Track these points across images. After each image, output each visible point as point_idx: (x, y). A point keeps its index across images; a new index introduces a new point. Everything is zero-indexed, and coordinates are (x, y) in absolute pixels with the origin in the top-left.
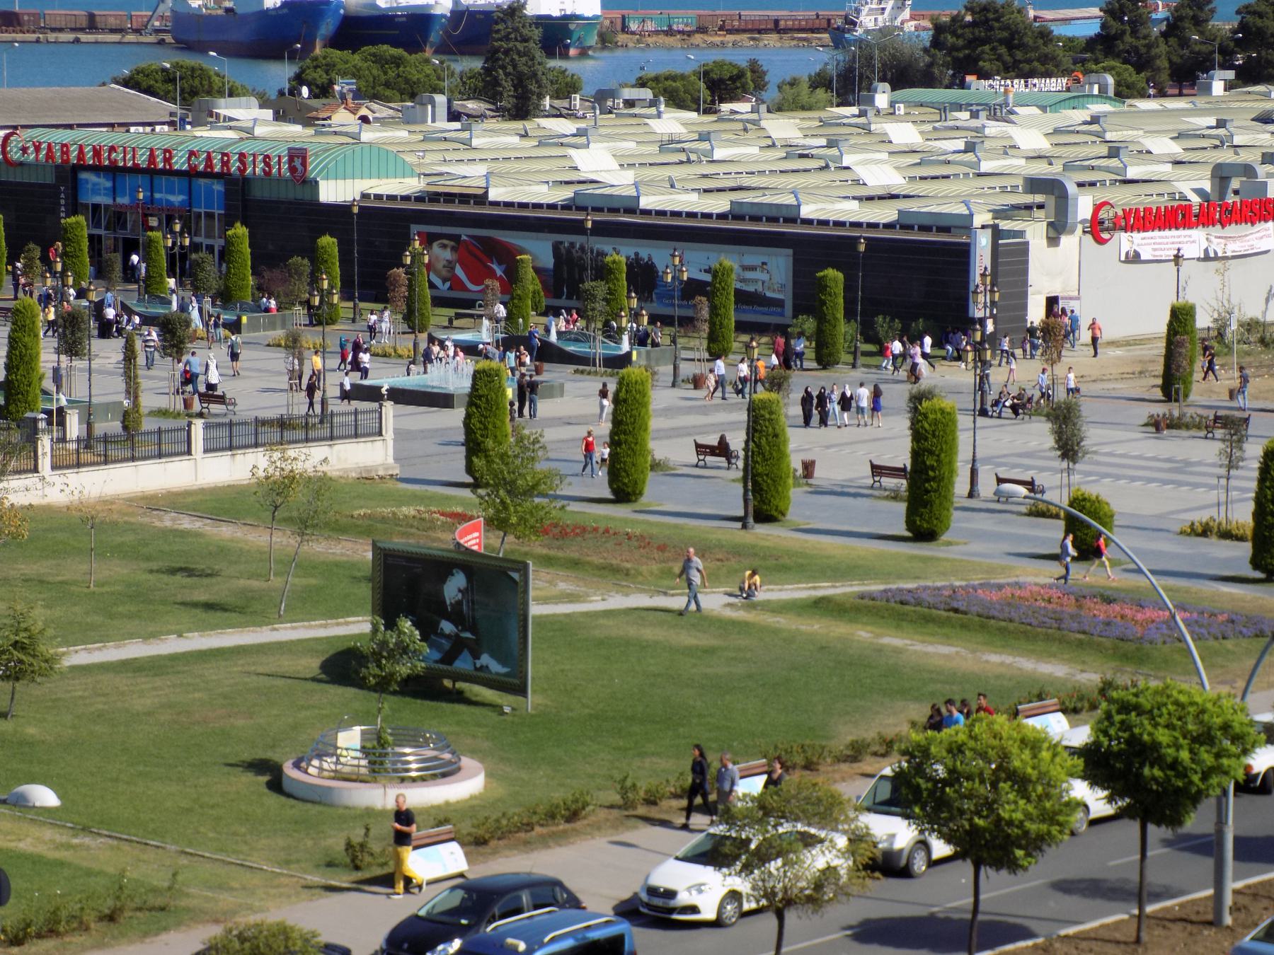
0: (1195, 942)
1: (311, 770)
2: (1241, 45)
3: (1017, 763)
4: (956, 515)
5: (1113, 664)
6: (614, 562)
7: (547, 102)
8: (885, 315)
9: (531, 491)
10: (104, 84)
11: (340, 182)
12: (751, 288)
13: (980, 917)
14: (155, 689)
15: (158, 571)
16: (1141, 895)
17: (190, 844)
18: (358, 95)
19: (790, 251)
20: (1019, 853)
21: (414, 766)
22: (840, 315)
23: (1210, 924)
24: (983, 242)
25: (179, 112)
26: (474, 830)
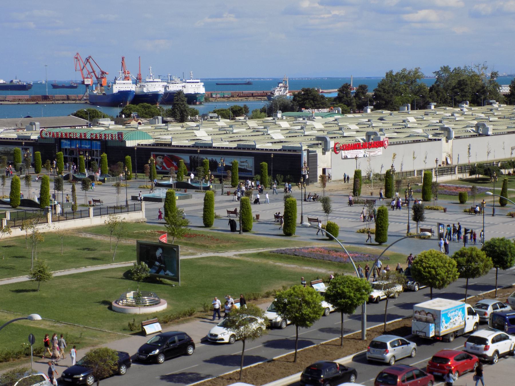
0: (357, 345)
1: (120, 304)
2: (375, 99)
3: (307, 298)
4: (297, 228)
5: (337, 269)
6: (204, 244)
7: (189, 117)
8: (279, 174)
9: (180, 225)
10: (69, 115)
11: (132, 141)
12: (243, 168)
13: (299, 339)
14: (78, 282)
15: (81, 249)
16: (342, 331)
17: (86, 325)
18: (138, 117)
19: (253, 157)
20: (308, 323)
21: (148, 302)
22: (267, 174)
23: (361, 339)
24: (305, 154)
25: (89, 122)
26: (163, 319)
